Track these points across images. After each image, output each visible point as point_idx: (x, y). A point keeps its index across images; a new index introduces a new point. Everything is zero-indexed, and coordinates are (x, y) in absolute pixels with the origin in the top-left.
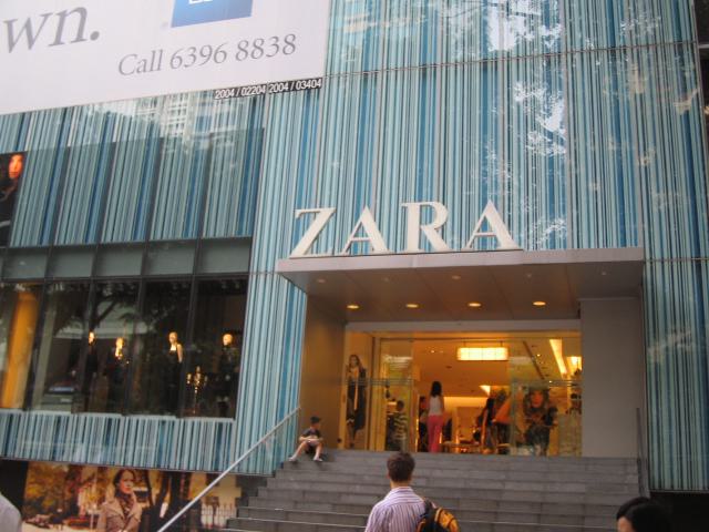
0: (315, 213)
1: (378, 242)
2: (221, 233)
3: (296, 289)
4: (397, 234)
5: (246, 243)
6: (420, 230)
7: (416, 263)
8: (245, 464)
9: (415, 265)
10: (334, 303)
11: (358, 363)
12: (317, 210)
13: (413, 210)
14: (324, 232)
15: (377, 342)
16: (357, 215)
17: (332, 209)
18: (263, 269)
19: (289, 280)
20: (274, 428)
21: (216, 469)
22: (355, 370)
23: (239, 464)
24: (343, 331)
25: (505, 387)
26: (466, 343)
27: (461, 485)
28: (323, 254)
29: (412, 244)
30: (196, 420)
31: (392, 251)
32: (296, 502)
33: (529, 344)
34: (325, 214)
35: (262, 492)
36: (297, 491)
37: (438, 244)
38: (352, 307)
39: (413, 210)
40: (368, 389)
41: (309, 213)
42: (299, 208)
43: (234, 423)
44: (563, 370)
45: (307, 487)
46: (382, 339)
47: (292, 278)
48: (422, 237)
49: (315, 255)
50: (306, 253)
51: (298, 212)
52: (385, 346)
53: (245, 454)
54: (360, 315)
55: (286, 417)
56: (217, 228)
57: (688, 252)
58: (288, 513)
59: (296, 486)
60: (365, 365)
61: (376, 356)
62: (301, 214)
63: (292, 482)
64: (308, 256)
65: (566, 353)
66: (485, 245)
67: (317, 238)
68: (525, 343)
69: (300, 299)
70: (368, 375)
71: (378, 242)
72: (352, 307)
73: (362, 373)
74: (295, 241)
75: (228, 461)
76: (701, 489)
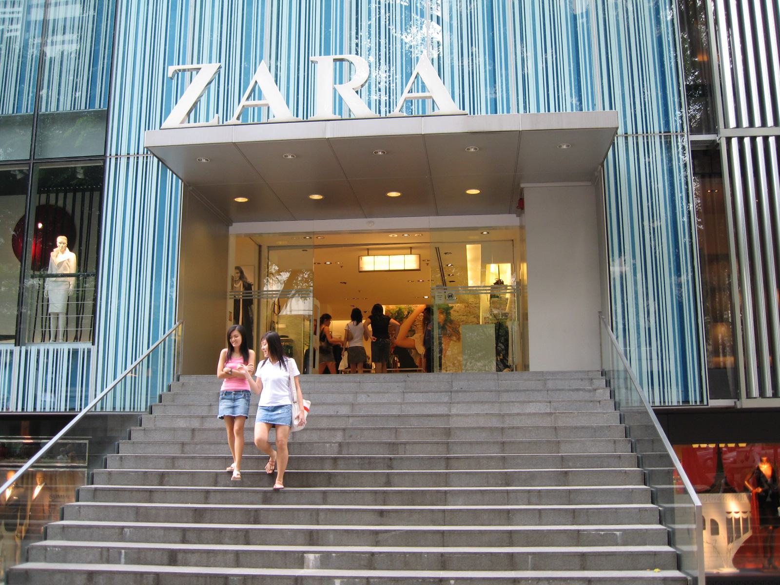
0: (191, 70)
1: (276, 102)
2: (66, 106)
3: (169, 173)
4: (303, 97)
5: (103, 117)
6: (335, 90)
7: (331, 131)
8: (99, 405)
9: (329, 135)
10: (221, 194)
11: (242, 276)
12: (195, 66)
13: (324, 66)
14: (204, 100)
15: (265, 250)
16: (246, 74)
17: (215, 66)
18: (124, 152)
19: (159, 160)
20: (146, 352)
21: (72, 409)
22: (239, 285)
23: (102, 399)
24: (228, 229)
25: (403, 306)
26: (369, 249)
27: (395, 411)
28: (203, 123)
29: (323, 107)
30: (43, 348)
31: (300, 118)
32: (183, 444)
33: (442, 252)
34: (208, 70)
35: (137, 435)
36: (184, 429)
37: (358, 106)
38: (240, 200)
39: (324, 66)
40: (255, 307)
41: (184, 70)
42: (172, 65)
43: (94, 349)
44: (472, 281)
45: (196, 424)
46: (269, 248)
47: (163, 156)
48: (338, 102)
49: (192, 124)
50: (182, 122)
51: (171, 70)
52: (273, 254)
53: (110, 386)
54: (249, 212)
55: (161, 337)
56: (60, 98)
57: (656, 126)
58: (174, 458)
59: (181, 423)
60: (250, 278)
61: (264, 265)
62: (177, 72)
63: (174, 420)
64: (186, 125)
65: (486, 260)
66: (420, 107)
67: (195, 105)
68: (437, 249)
69: (175, 188)
70: (255, 288)
71: (276, 102)
72: (240, 200)
73: (248, 287)
74: (166, 111)
75: (87, 397)
76: (63, 409)
